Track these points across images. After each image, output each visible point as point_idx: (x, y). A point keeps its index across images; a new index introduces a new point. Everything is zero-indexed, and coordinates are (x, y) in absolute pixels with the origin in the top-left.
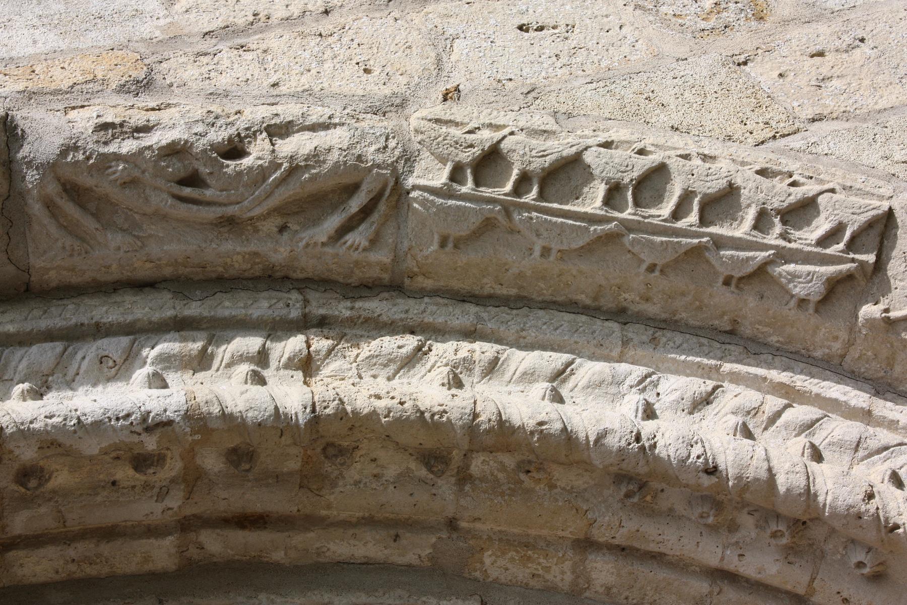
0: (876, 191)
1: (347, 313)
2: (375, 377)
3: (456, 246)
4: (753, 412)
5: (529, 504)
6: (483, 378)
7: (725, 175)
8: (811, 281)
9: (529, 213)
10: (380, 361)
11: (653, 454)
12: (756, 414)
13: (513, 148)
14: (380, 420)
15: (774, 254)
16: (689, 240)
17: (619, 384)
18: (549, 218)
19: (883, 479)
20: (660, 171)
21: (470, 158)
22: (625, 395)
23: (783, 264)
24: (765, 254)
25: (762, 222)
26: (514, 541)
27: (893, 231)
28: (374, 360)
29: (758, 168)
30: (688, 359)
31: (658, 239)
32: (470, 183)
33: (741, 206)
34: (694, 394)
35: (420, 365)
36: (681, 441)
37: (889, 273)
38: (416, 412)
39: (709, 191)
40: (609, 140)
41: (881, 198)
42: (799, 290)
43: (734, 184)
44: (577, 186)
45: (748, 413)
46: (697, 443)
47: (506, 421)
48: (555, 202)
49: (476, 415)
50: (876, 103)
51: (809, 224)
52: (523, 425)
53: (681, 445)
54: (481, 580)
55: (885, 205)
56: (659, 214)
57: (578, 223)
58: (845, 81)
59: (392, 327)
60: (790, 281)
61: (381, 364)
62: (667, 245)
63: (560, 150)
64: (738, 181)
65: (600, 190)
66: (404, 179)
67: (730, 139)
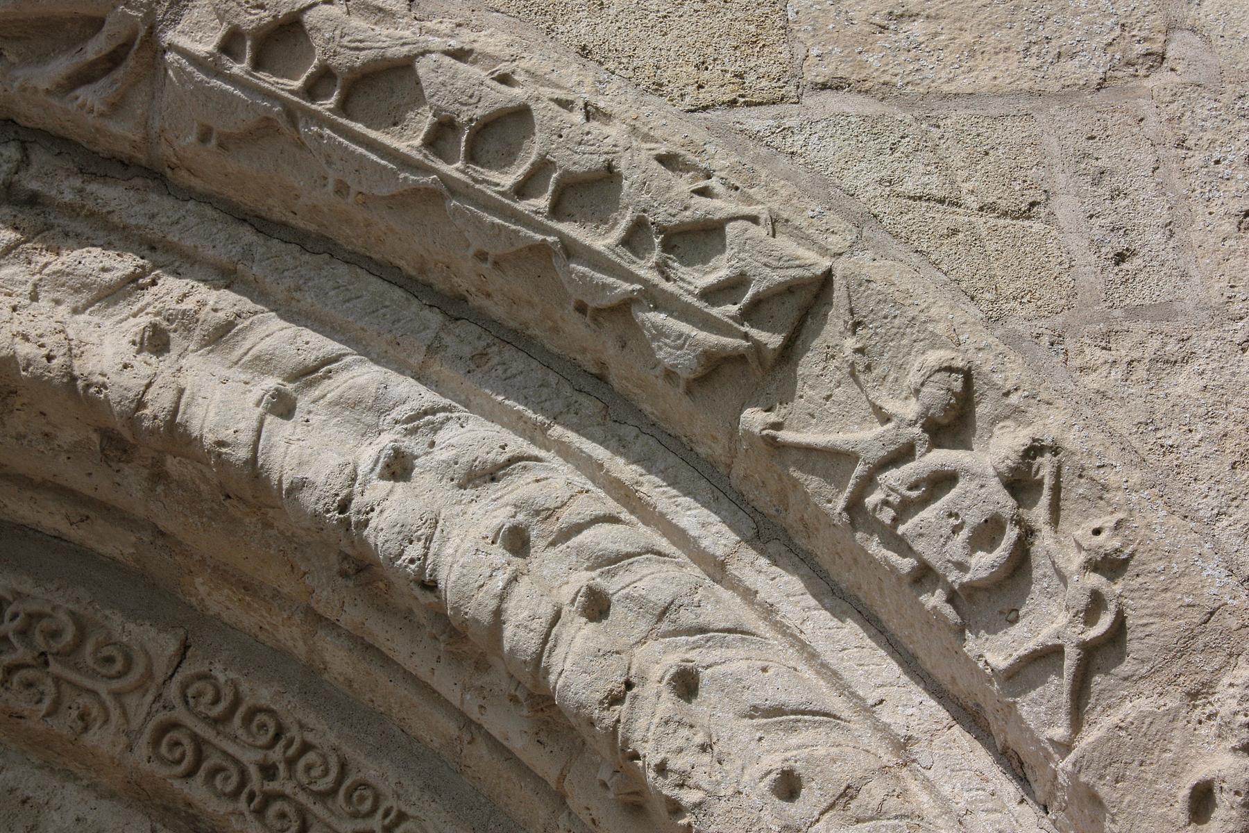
0: (820, 238)
1: (68, 197)
2: (58, 302)
3: (221, 145)
4: (544, 514)
5: (231, 539)
6: (202, 347)
7: (606, 149)
8: (681, 347)
9: (321, 127)
10: (71, 283)
11: (360, 535)
12: (547, 518)
13: (319, 25)
14: (19, 372)
15: (639, 291)
16: (531, 233)
17: (382, 412)
18: (346, 142)
19: (662, 678)
20: (521, 115)
21: (254, 25)
22: (383, 430)
23: (650, 310)
24: (628, 287)
25: (635, 238)
26: (233, 576)
27: (824, 309)
28: (64, 279)
29: (663, 150)
30: (507, 402)
31: (490, 218)
32: (246, 64)
33: (618, 203)
34: (475, 461)
35: (125, 303)
36: (397, 529)
37: (800, 371)
38: (63, 376)
39: (574, 168)
40: (467, 47)
41: (824, 251)
42: (665, 355)
43: (615, 167)
44: (399, 106)
45: (537, 513)
46: (419, 540)
47: (180, 424)
48: (360, 122)
49: (141, 404)
50: (950, 80)
51: (705, 261)
52: (201, 437)
53: (395, 536)
54: (198, 608)
55: (826, 263)
56: (498, 181)
57: (383, 162)
58: (932, 27)
59: (125, 234)
60: (655, 338)
61: (71, 287)
62: (500, 231)
63: (384, 45)
64: (622, 165)
65: (424, 121)
66: (161, 31)
67: (656, 90)
